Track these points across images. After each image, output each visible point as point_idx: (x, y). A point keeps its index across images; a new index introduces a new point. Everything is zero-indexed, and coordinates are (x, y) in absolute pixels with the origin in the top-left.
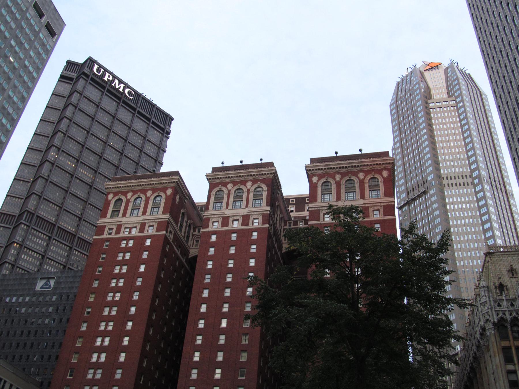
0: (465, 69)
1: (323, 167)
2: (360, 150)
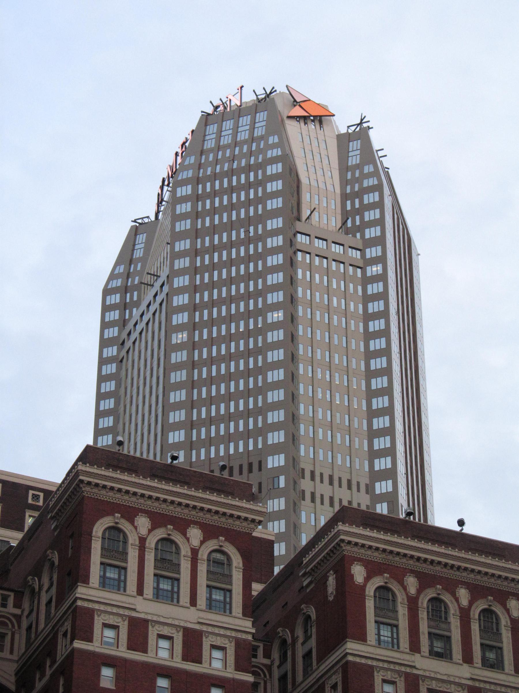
0: (380, 154)
1: (382, 546)
2: (461, 523)
